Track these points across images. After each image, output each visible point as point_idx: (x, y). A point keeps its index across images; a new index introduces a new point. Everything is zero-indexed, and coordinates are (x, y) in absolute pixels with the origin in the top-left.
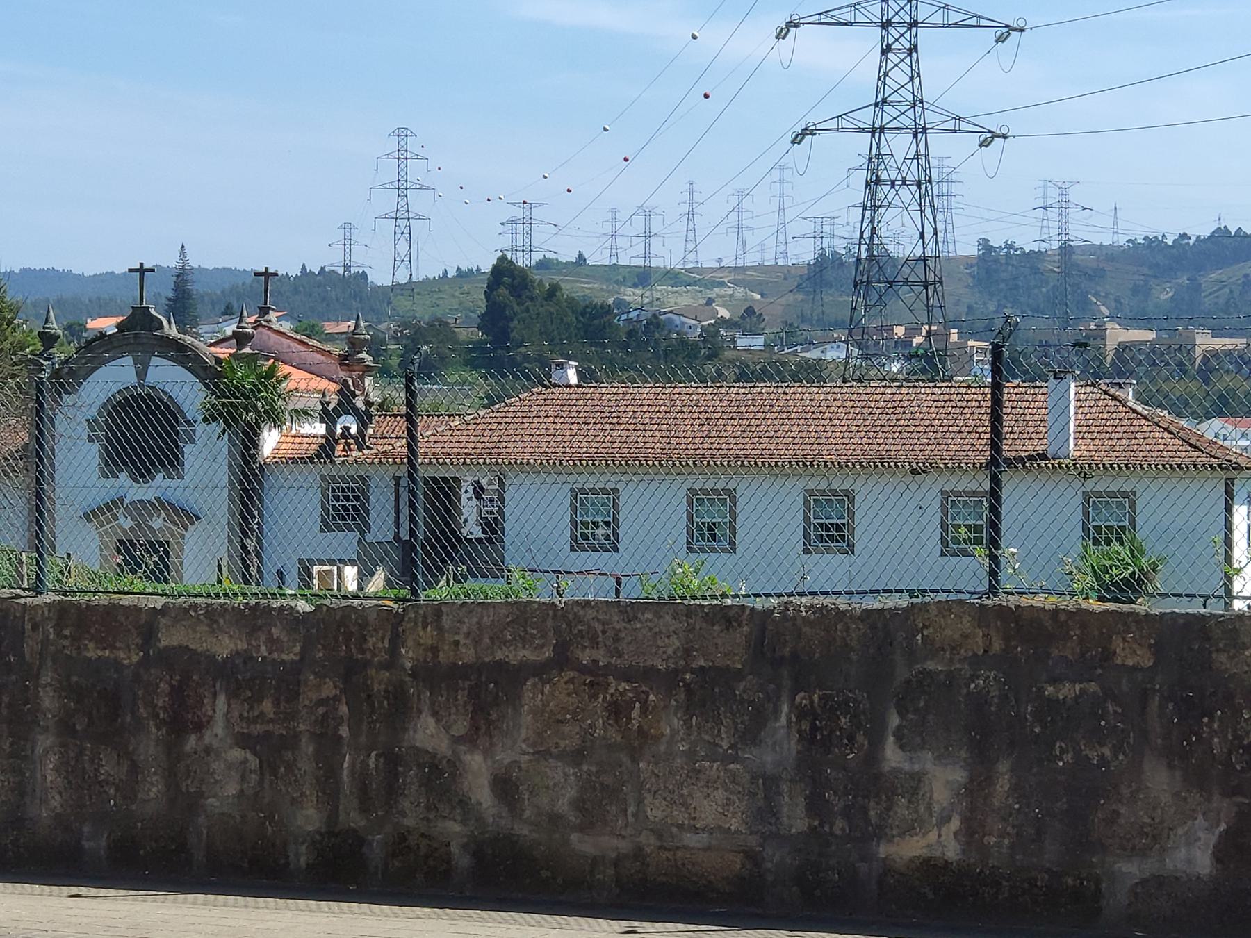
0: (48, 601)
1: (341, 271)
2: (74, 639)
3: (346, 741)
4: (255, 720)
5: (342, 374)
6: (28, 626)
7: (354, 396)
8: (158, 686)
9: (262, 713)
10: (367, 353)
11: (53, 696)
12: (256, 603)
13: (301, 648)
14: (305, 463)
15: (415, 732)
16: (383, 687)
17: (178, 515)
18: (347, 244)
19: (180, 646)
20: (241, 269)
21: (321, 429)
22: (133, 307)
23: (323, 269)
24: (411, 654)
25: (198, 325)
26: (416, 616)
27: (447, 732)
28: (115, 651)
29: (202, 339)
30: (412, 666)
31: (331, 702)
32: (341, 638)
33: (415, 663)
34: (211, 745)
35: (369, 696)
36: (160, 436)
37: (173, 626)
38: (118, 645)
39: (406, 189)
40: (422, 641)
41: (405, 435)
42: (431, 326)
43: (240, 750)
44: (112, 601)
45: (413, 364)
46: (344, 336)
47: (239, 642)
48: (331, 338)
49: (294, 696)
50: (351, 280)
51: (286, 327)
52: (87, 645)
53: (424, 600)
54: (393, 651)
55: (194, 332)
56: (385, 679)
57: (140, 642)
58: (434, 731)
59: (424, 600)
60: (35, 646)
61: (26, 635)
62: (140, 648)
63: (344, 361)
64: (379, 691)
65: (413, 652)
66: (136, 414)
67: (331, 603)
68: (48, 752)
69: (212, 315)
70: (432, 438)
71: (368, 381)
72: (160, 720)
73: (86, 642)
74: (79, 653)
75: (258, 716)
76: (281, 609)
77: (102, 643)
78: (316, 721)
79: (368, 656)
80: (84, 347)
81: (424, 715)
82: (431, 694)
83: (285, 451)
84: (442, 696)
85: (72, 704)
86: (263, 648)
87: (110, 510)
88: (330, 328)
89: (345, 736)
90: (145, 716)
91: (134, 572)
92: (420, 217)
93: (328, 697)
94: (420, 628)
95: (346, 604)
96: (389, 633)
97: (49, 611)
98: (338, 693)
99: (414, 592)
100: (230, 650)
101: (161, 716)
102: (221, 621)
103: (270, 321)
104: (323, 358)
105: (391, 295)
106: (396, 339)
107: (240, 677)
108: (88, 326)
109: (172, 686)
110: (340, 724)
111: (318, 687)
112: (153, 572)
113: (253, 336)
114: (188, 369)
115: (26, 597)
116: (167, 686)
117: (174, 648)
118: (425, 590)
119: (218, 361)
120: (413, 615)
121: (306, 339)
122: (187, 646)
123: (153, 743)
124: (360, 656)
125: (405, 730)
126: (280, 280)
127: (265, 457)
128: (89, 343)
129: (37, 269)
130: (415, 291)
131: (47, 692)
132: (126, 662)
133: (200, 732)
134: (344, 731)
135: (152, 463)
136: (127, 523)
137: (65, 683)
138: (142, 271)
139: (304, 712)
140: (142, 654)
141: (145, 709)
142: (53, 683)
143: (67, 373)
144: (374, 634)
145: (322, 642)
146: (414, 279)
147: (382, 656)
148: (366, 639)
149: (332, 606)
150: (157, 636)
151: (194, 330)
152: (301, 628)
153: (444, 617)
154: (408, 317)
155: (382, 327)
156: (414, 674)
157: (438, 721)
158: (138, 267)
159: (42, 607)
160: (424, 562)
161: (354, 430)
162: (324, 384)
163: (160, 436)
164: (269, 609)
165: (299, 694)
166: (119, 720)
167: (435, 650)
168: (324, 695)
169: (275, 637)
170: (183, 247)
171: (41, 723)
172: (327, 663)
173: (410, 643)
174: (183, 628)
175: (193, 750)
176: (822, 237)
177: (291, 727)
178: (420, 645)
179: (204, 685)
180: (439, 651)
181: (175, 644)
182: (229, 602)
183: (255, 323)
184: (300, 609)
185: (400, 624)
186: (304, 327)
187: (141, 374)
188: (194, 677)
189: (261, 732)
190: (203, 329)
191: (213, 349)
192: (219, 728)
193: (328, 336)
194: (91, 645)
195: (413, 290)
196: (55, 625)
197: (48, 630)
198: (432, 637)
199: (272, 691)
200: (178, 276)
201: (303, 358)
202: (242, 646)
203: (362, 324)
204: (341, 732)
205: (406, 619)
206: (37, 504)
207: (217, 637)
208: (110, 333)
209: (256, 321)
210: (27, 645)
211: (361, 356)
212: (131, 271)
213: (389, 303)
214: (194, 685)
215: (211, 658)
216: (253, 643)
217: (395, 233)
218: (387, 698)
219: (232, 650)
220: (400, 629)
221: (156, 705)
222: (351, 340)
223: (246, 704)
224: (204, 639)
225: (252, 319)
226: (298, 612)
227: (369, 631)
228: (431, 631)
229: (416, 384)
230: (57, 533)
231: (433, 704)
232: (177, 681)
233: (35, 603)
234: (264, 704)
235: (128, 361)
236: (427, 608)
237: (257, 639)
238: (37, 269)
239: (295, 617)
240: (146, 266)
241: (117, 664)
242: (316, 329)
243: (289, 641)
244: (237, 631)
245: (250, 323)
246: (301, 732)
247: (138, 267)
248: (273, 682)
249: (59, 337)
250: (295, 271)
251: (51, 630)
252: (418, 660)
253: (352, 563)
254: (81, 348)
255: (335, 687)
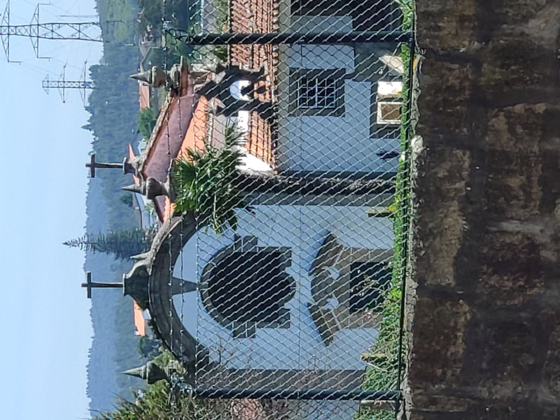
0: (409, 389)
1: (89, 91)
2: (445, 365)
3: (550, 106)
4: (528, 195)
5: (190, 94)
6: (433, 408)
7: (212, 83)
8: (492, 286)
9: (522, 187)
10: (170, 70)
11: (501, 385)
12: (414, 192)
13: (458, 149)
14: (276, 124)
15: (542, 39)
16: (497, 70)
17: (327, 248)
18: (63, 85)
19: (454, 264)
20: (87, 187)
21: (243, 115)
22: (125, 294)
23: (87, 109)
24: (466, 43)
25: (142, 229)
26: (429, 38)
27: (544, 7)
28: (459, 327)
29: (155, 226)
30: (478, 41)
31: (511, 120)
32: (449, 111)
33: (474, 38)
34: (551, 236)
35: (507, 83)
36: (248, 274)
37: (435, 272)
38: (452, 324)
39: (9, 27)
40: (453, 32)
41: (250, 46)
42: (143, 5)
43: (556, 209)
44: (410, 330)
45: (181, 37)
46: (153, 89)
47: (452, 209)
48: (155, 101)
49: (506, 157)
50: (97, 81)
51: (144, 145)
52: (452, 354)
53: (413, 29)
54: (462, 59)
55: (149, 234)
56: (490, 67)
57: (449, 303)
58: (542, 20)
59: (413, 29)
60: (451, 402)
61: (441, 410)
62: (455, 303)
63: (177, 92)
64: (502, 74)
65: (464, 40)
66: (229, 304)
67: (415, 119)
68: (554, 390)
69: (132, 216)
70: (254, 7)
71: (197, 68)
72: (525, 284)
73: (449, 353)
74: (460, 360)
75: (524, 191)
76: (420, 168)
77: (450, 339)
78: (530, 135)
79: (467, 84)
80: (163, 341)
81: (527, 31)
82: (505, 24)
83: (266, 136)
84: (508, 12)
85: (508, 367)
86: (457, 185)
87: (322, 321)
88: (145, 102)
89: (545, 108)
90: (521, 299)
91: (381, 300)
92: (36, 14)
93: (506, 123)
94: (441, 34)
95: (416, 105)
96: (445, 63)
97: (418, 388)
98: (502, 113)
99: (405, 38)
100: (458, 218)
101: (521, 283)
102: (430, 225)
103: (138, 163)
104: (174, 112)
105: (112, 42)
106: (156, 39)
107: (486, 208)
108: (143, 334)
109: (494, 272)
110: (533, 112)
111: (497, 132)
112: (382, 281)
113: (153, 180)
114: (185, 242)
115: (405, 411)
116: (493, 277)
117: (456, 270)
118: (401, 29)
119: (176, 214)
120: (428, 40)
121: (156, 129)
122: (454, 258)
123: (548, 292)
124: (467, 92)
125: (540, 47)
126: (98, 151)
127: (270, 169)
128: (159, 336)
129: (88, 381)
130: (109, 20)
131: (496, 392)
132: (469, 316)
133: (538, 246)
134: (541, 108)
135: (275, 281)
136: (334, 303)
137: (489, 374)
138: (89, 285)
139: (519, 145)
140: (461, 301)
141: (514, 299)
142: (488, 385)
143: (189, 358)
144: (445, 78)
145: (452, 129)
146: (97, 20)
147: (467, 70)
148: (451, 86)
149: (417, 119)
150: (444, 287)
151: (147, 234)
152: (438, 148)
153: (430, 9)
154: (134, 26)
155: (144, 52)
156: (485, 39)
157: (532, 16)
158: (89, 168)
159: (414, 395)
160: (376, 29)
161: (245, 83)
162: (199, 114)
163: (248, 274)
164: (419, 179)
165: (504, 151)
166: (525, 323)
167: (462, 19)
168: (506, 127)
169: (446, 174)
170: (66, 244)
171: (526, 396)
172: (474, 124)
173: (454, 43)
174: (437, 262)
175: (556, 253)
176: (48, 81)
177: (535, 158)
178: (457, 34)
179: (492, 242)
180: (464, 15)
181: (451, 269)
182: (412, 218)
183: (140, 178)
184: (420, 150)
185: (435, 53)
186: (144, 128)
187: (189, 287)
188: (484, 252)
189: (540, 188)
190: (146, 226)
191: (165, 219)
192: (535, 228)
193: (152, 105)
194: (452, 349)
195: (108, 22)
196: (432, 382)
197: (437, 389)
198: (449, 22)
199: (500, 177)
200: (95, 248)
201: (174, 132)
202: (455, 206)
203: (141, 74)
204: (541, 111)
205: (431, 46)
206: (315, 399)
207: (446, 229)
208: (149, 315)
209: (138, 176)
210: (451, 409)
211: (172, 76)
212: (89, 296)
213: (121, 45)
214: (492, 252)
215: (466, 235)
216: (452, 194)
217: (52, 38)
218: (509, 66)
219: (459, 216)
220: (441, 52)
221: (511, 288)
222: (157, 84)
223: (512, 203)
224: (448, 242)
225: (137, 180)
226: (422, 152)
227: (442, 83)
228: (444, 23)
229: (200, 35)
230: (315, 67)
231: (515, 22)
232: (487, 269)
233: (411, 401)
234: (512, 185)
235: (177, 299)
236: (421, 27)
237: (448, 191)
238: (88, 381)
239: (428, 154)
240: (86, 282)
241: (472, 325)
242: (146, 116)
243: (451, 161)
244: (441, 210)
245: (140, 183)
246: (540, 150)
247: (89, 168)
248: (491, 176)
249: (153, 365)
250: (90, 136)
251: (437, 386)
252: (472, 35)
253: (374, 89)
254: (164, 343)
255: (496, 116)
